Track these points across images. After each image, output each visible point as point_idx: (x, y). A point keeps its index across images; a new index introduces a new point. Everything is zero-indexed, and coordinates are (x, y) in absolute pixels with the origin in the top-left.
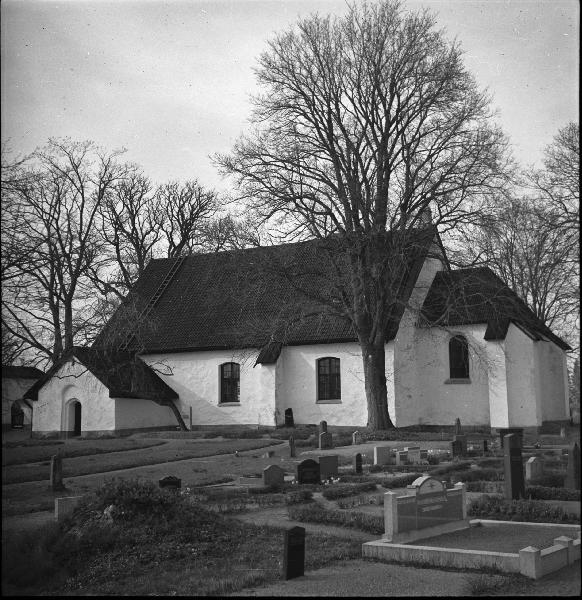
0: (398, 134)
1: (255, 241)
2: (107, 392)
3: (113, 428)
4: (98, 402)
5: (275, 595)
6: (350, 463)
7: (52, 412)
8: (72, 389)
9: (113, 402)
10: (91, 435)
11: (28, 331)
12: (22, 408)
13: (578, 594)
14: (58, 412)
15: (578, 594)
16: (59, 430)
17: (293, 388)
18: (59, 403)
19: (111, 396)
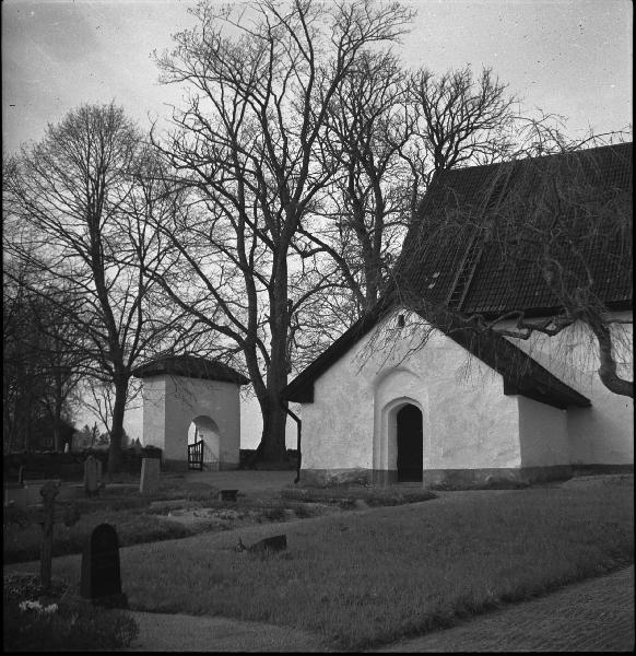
0: (244, 218)
1: (559, 138)
2: (496, 382)
3: (516, 463)
4: (472, 406)
5: (301, 651)
6: (76, 551)
7: (349, 426)
8: (399, 377)
9: (513, 403)
10: (456, 480)
11: (210, 129)
12: (524, 345)
13: (632, 650)
14: (367, 428)
15: (632, 650)
16: (370, 467)
17: (323, 478)
18: (367, 408)
19: (509, 390)
